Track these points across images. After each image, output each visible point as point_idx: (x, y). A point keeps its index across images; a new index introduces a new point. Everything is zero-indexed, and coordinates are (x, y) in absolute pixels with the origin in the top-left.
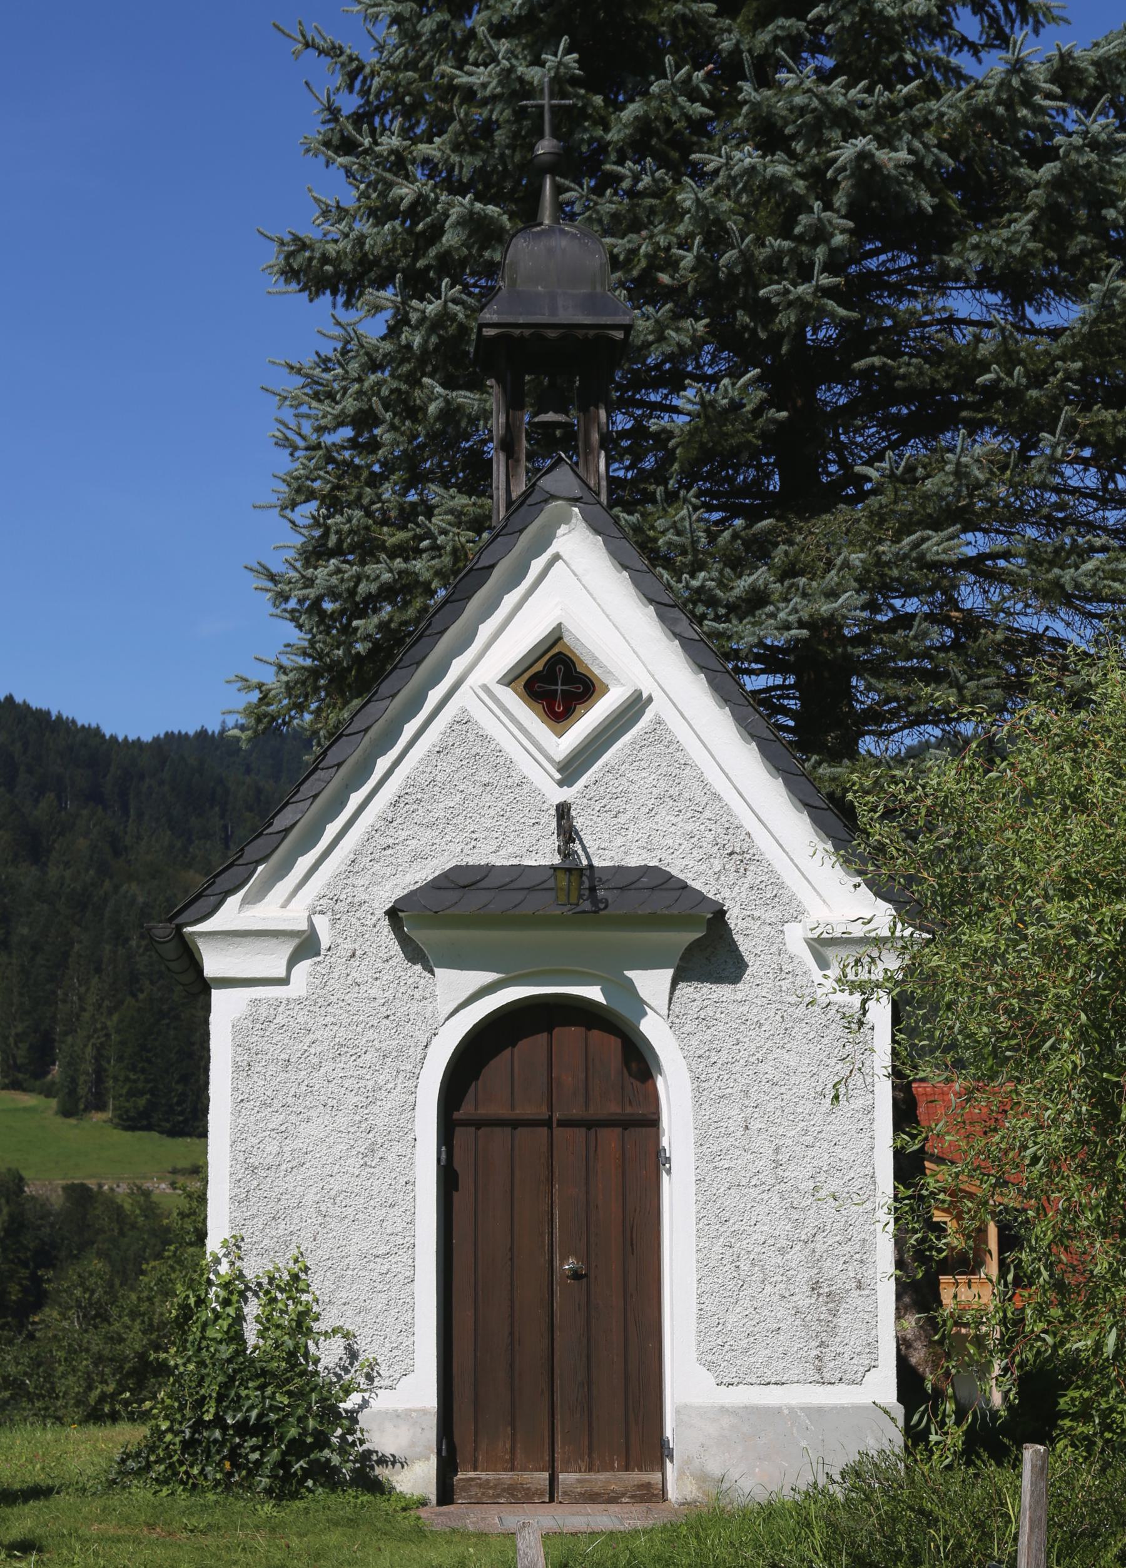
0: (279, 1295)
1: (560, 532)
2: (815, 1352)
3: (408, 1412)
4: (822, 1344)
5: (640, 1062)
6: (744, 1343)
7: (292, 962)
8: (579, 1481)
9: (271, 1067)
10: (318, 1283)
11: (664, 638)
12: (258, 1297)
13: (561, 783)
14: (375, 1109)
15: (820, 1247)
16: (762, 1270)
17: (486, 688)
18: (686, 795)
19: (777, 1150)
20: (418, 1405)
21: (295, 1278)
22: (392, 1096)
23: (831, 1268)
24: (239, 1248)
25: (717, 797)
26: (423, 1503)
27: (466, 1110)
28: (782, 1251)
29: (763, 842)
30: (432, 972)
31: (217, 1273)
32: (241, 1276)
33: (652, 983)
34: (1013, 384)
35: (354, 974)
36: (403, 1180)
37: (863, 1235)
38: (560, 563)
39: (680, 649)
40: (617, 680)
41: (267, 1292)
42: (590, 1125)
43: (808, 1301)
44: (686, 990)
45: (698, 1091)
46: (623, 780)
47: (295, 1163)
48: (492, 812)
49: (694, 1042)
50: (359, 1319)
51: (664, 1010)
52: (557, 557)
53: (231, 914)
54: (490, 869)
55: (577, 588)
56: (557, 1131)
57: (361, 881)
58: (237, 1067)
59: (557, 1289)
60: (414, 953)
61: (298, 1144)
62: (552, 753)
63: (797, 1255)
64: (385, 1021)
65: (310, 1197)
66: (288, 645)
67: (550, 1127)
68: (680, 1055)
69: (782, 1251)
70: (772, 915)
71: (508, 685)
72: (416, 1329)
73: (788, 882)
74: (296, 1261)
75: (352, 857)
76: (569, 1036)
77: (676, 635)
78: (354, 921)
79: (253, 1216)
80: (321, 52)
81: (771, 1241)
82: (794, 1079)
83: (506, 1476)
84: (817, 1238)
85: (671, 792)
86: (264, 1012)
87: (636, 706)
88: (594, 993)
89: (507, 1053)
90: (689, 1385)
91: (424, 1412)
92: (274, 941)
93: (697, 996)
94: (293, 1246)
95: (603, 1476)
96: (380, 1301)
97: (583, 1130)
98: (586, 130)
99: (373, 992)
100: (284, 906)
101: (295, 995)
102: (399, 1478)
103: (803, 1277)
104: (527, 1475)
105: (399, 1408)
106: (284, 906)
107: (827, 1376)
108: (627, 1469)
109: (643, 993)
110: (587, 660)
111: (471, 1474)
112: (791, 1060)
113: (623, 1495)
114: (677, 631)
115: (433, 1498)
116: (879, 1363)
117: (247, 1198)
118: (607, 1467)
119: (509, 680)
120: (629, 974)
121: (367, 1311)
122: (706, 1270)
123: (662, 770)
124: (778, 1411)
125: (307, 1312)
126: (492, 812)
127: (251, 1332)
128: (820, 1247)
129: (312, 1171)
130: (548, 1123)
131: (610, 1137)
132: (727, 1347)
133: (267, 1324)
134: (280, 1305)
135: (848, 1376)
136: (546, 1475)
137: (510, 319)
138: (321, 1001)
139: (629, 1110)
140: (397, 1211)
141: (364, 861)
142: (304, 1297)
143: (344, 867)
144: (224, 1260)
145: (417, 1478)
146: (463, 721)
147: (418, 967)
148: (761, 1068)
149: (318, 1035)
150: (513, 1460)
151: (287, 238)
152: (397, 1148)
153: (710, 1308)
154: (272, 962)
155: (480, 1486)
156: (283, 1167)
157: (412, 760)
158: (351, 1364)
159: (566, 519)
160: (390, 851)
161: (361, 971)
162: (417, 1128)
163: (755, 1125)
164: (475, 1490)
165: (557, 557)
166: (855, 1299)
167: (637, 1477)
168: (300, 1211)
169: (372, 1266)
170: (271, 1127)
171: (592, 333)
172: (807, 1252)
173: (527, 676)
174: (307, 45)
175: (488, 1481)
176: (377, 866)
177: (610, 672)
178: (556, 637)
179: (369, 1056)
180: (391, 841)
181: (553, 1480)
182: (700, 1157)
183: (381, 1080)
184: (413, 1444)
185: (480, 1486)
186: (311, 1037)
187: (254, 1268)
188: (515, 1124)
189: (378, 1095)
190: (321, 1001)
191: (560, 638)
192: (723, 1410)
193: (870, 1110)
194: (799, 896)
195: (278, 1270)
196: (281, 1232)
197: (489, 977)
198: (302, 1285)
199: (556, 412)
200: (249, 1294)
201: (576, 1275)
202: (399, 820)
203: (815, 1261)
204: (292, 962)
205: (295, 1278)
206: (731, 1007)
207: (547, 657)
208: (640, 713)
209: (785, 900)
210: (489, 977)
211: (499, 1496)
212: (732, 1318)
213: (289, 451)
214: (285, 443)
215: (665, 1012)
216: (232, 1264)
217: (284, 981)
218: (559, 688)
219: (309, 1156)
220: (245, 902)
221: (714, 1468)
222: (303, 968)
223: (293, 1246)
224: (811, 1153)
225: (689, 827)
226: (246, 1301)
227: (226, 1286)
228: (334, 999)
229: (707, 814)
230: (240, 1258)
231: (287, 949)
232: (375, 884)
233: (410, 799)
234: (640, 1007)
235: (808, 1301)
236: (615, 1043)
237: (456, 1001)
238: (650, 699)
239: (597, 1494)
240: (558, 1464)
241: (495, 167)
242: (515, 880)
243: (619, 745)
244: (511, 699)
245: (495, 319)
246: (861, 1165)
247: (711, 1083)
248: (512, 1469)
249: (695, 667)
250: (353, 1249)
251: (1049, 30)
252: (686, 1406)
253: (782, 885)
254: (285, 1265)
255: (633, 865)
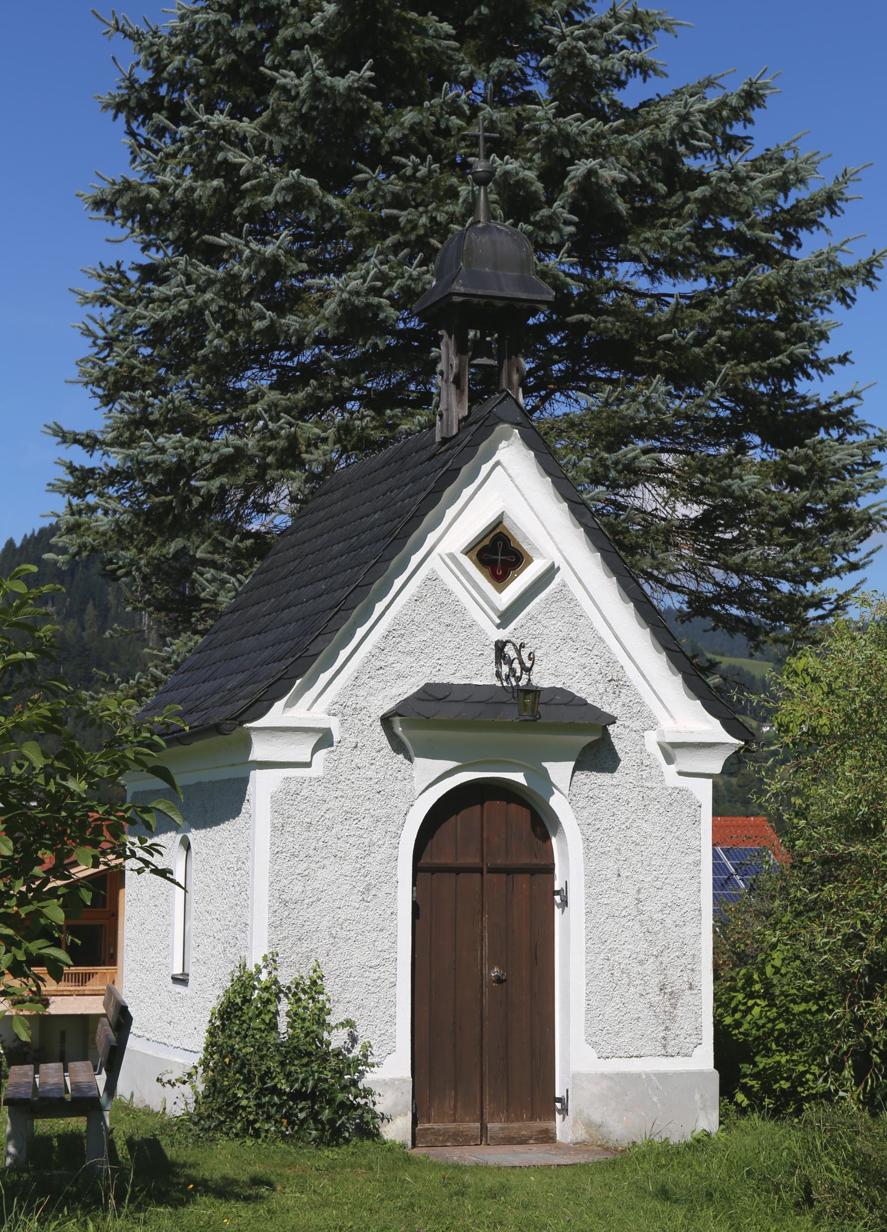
0: (303, 997)
1: (501, 446)
2: (662, 1034)
3: (393, 1080)
4: (667, 1028)
5: (543, 825)
6: (616, 1028)
7: (315, 750)
8: (501, 1129)
9: (297, 828)
10: (330, 986)
11: (571, 526)
12: (288, 998)
13: (499, 626)
14: (370, 859)
15: (665, 960)
16: (628, 976)
17: (452, 556)
18: (581, 638)
19: (639, 891)
20: (398, 1076)
21: (314, 983)
22: (382, 850)
23: (673, 974)
24: (275, 961)
25: (601, 640)
26: (403, 1146)
27: (424, 860)
28: (641, 963)
29: (631, 673)
30: (410, 760)
31: (259, 980)
32: (276, 982)
33: (559, 771)
34: (683, 343)
35: (357, 760)
36: (389, 912)
37: (693, 952)
38: (499, 468)
39: (583, 534)
40: (541, 554)
41: (295, 994)
42: (509, 871)
43: (658, 998)
44: (581, 776)
45: (588, 848)
46: (539, 626)
47: (314, 899)
48: (452, 645)
49: (585, 814)
50: (358, 1014)
51: (567, 791)
52: (498, 463)
53: (278, 714)
54: (450, 686)
55: (510, 486)
56: (487, 876)
57: (361, 692)
58: (274, 828)
59: (486, 990)
60: (398, 746)
61: (316, 885)
62: (497, 604)
63: (650, 966)
64: (378, 796)
65: (325, 923)
66: (49, 485)
67: (482, 874)
68: (575, 823)
69: (641, 963)
70: (636, 725)
71: (466, 554)
72: (397, 1020)
73: (647, 702)
74: (315, 971)
75: (356, 674)
76: (495, 807)
77: (583, 525)
78: (356, 721)
79: (285, 938)
80: (126, 35)
81: (634, 956)
82: (649, 841)
83: (451, 1126)
84: (665, 953)
85: (572, 635)
86: (293, 787)
87: (551, 573)
88: (519, 777)
89: (453, 818)
90: (577, 1057)
91: (403, 1080)
92: (305, 735)
93: (587, 781)
94: (313, 959)
95: (516, 1125)
96: (372, 1000)
97: (504, 875)
98: (369, 128)
99: (370, 774)
100: (309, 710)
101: (315, 775)
102: (386, 1129)
103: (655, 981)
104: (465, 1125)
105: (389, 1076)
106: (309, 710)
107: (670, 1051)
108: (532, 1118)
109: (553, 779)
110: (519, 539)
111: (427, 1126)
112: (647, 827)
113: (530, 1138)
114: (584, 521)
115: (410, 1143)
116: (703, 1041)
117: (281, 925)
118: (519, 1118)
119: (467, 552)
120: (545, 764)
121: (364, 1007)
122: (592, 976)
123: (566, 619)
124: (639, 1075)
125: (321, 1009)
126: (452, 645)
127: (283, 1023)
128: (665, 960)
129: (326, 905)
130: (480, 871)
131: (522, 881)
132: (605, 1031)
133: (294, 1016)
134: (304, 1003)
135: (683, 1051)
136: (478, 1125)
137: (473, 292)
138: (333, 780)
139: (535, 861)
140: (385, 934)
141: (364, 678)
142: (321, 997)
143: (350, 682)
144: (265, 971)
145: (397, 1129)
146: (433, 579)
147: (401, 756)
148: (629, 833)
149: (331, 805)
150: (454, 1115)
151: (119, 180)
152: (385, 888)
153: (594, 1004)
154: (300, 750)
155: (433, 1134)
156: (306, 902)
157: (397, 607)
158: (353, 1046)
159: (507, 438)
160: (381, 671)
161: (360, 759)
162: (398, 874)
163: (624, 873)
164: (430, 1137)
165: (498, 463)
166: (688, 997)
167: (540, 1125)
168: (318, 934)
169: (367, 974)
170: (298, 871)
171: (526, 305)
172: (657, 963)
173: (478, 548)
174: (117, 29)
175: (439, 1130)
176: (372, 682)
177: (536, 548)
178: (499, 522)
179: (366, 821)
180: (383, 664)
181: (484, 1128)
182: (588, 896)
183: (375, 838)
184: (396, 1104)
185: (433, 1134)
186: (326, 806)
187: (285, 978)
188: (458, 870)
189: (372, 849)
190: (333, 780)
191: (501, 522)
192: (603, 1076)
193: (698, 863)
194: (654, 712)
195: (302, 977)
196: (304, 949)
197: (451, 764)
198: (319, 989)
199: (489, 358)
200: (281, 995)
201: (499, 980)
202: (388, 649)
203: (662, 970)
204: (315, 750)
205: (314, 983)
206: (610, 789)
207: (492, 535)
208: (552, 578)
209: (646, 714)
210: (451, 764)
211: (447, 1141)
212: (608, 1010)
213: (91, 340)
214: (87, 332)
215: (566, 792)
216: (270, 973)
217: (308, 765)
218: (499, 557)
219: (324, 894)
220: (288, 705)
221: (597, 1118)
222: (322, 753)
223: (313, 959)
224: (661, 893)
225: (583, 661)
226: (279, 1000)
227: (266, 989)
228: (342, 778)
229: (595, 652)
230: (275, 969)
231: (313, 740)
232: (371, 695)
233: (396, 634)
234: (550, 787)
235: (658, 998)
236: (526, 813)
237: (428, 781)
238: (559, 569)
239: (513, 1138)
240: (486, 1117)
241: (296, 146)
242: (468, 695)
243: (537, 600)
244: (467, 563)
245: (462, 290)
246: (692, 902)
247: (596, 843)
248: (454, 1121)
249: (593, 547)
250: (354, 962)
251: (653, 79)
252: (579, 1074)
253: (642, 704)
254: (306, 973)
255: (545, 686)
